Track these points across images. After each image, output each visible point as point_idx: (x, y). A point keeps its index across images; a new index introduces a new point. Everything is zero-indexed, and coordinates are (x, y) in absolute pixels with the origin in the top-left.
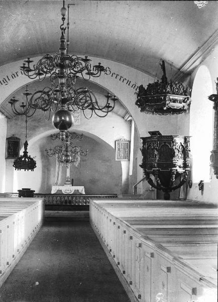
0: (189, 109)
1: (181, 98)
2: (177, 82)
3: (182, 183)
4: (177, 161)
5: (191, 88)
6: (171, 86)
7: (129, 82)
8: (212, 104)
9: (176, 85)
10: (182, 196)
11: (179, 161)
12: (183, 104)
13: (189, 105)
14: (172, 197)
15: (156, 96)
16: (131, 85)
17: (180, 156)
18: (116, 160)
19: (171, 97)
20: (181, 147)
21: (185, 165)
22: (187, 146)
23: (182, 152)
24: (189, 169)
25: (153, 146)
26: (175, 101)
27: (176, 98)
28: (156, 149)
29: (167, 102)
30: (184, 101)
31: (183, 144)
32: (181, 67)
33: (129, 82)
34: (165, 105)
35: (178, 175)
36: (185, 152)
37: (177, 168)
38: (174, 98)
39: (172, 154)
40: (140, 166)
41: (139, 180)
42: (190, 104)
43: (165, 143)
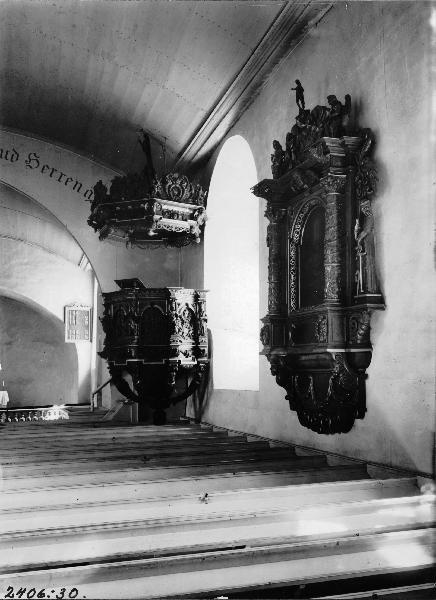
0: (202, 235)
1: (184, 208)
2: (176, 175)
3: (190, 391)
4: (179, 343)
5: (206, 189)
6: (164, 183)
7: (78, 186)
8: (258, 205)
9: (175, 180)
10: (190, 412)
11: (185, 344)
12: (192, 222)
13: (202, 228)
14: (169, 416)
15: (132, 204)
16: (83, 191)
17: (186, 331)
18: (67, 341)
19: (164, 207)
20: (187, 312)
21: (197, 352)
22: (200, 310)
23: (190, 323)
24: (205, 359)
25: (127, 311)
26: (172, 215)
27: (175, 209)
28: (134, 318)
29: (156, 217)
30: (192, 217)
31: (191, 307)
32: (176, 160)
33: (78, 186)
34: (150, 222)
35: (184, 372)
36: (196, 319)
37: (181, 357)
38: (171, 208)
39: (170, 329)
40: (101, 182)
41: (104, 382)
42: (204, 225)
43: (152, 304)
